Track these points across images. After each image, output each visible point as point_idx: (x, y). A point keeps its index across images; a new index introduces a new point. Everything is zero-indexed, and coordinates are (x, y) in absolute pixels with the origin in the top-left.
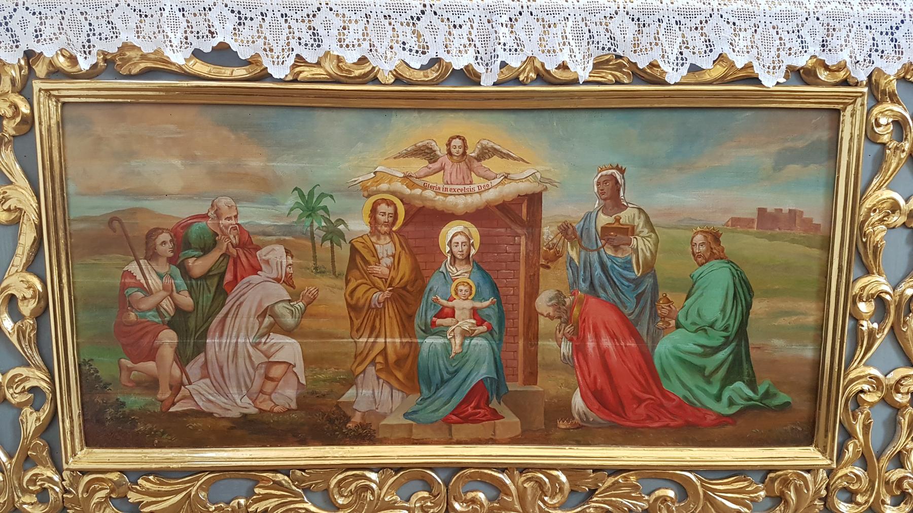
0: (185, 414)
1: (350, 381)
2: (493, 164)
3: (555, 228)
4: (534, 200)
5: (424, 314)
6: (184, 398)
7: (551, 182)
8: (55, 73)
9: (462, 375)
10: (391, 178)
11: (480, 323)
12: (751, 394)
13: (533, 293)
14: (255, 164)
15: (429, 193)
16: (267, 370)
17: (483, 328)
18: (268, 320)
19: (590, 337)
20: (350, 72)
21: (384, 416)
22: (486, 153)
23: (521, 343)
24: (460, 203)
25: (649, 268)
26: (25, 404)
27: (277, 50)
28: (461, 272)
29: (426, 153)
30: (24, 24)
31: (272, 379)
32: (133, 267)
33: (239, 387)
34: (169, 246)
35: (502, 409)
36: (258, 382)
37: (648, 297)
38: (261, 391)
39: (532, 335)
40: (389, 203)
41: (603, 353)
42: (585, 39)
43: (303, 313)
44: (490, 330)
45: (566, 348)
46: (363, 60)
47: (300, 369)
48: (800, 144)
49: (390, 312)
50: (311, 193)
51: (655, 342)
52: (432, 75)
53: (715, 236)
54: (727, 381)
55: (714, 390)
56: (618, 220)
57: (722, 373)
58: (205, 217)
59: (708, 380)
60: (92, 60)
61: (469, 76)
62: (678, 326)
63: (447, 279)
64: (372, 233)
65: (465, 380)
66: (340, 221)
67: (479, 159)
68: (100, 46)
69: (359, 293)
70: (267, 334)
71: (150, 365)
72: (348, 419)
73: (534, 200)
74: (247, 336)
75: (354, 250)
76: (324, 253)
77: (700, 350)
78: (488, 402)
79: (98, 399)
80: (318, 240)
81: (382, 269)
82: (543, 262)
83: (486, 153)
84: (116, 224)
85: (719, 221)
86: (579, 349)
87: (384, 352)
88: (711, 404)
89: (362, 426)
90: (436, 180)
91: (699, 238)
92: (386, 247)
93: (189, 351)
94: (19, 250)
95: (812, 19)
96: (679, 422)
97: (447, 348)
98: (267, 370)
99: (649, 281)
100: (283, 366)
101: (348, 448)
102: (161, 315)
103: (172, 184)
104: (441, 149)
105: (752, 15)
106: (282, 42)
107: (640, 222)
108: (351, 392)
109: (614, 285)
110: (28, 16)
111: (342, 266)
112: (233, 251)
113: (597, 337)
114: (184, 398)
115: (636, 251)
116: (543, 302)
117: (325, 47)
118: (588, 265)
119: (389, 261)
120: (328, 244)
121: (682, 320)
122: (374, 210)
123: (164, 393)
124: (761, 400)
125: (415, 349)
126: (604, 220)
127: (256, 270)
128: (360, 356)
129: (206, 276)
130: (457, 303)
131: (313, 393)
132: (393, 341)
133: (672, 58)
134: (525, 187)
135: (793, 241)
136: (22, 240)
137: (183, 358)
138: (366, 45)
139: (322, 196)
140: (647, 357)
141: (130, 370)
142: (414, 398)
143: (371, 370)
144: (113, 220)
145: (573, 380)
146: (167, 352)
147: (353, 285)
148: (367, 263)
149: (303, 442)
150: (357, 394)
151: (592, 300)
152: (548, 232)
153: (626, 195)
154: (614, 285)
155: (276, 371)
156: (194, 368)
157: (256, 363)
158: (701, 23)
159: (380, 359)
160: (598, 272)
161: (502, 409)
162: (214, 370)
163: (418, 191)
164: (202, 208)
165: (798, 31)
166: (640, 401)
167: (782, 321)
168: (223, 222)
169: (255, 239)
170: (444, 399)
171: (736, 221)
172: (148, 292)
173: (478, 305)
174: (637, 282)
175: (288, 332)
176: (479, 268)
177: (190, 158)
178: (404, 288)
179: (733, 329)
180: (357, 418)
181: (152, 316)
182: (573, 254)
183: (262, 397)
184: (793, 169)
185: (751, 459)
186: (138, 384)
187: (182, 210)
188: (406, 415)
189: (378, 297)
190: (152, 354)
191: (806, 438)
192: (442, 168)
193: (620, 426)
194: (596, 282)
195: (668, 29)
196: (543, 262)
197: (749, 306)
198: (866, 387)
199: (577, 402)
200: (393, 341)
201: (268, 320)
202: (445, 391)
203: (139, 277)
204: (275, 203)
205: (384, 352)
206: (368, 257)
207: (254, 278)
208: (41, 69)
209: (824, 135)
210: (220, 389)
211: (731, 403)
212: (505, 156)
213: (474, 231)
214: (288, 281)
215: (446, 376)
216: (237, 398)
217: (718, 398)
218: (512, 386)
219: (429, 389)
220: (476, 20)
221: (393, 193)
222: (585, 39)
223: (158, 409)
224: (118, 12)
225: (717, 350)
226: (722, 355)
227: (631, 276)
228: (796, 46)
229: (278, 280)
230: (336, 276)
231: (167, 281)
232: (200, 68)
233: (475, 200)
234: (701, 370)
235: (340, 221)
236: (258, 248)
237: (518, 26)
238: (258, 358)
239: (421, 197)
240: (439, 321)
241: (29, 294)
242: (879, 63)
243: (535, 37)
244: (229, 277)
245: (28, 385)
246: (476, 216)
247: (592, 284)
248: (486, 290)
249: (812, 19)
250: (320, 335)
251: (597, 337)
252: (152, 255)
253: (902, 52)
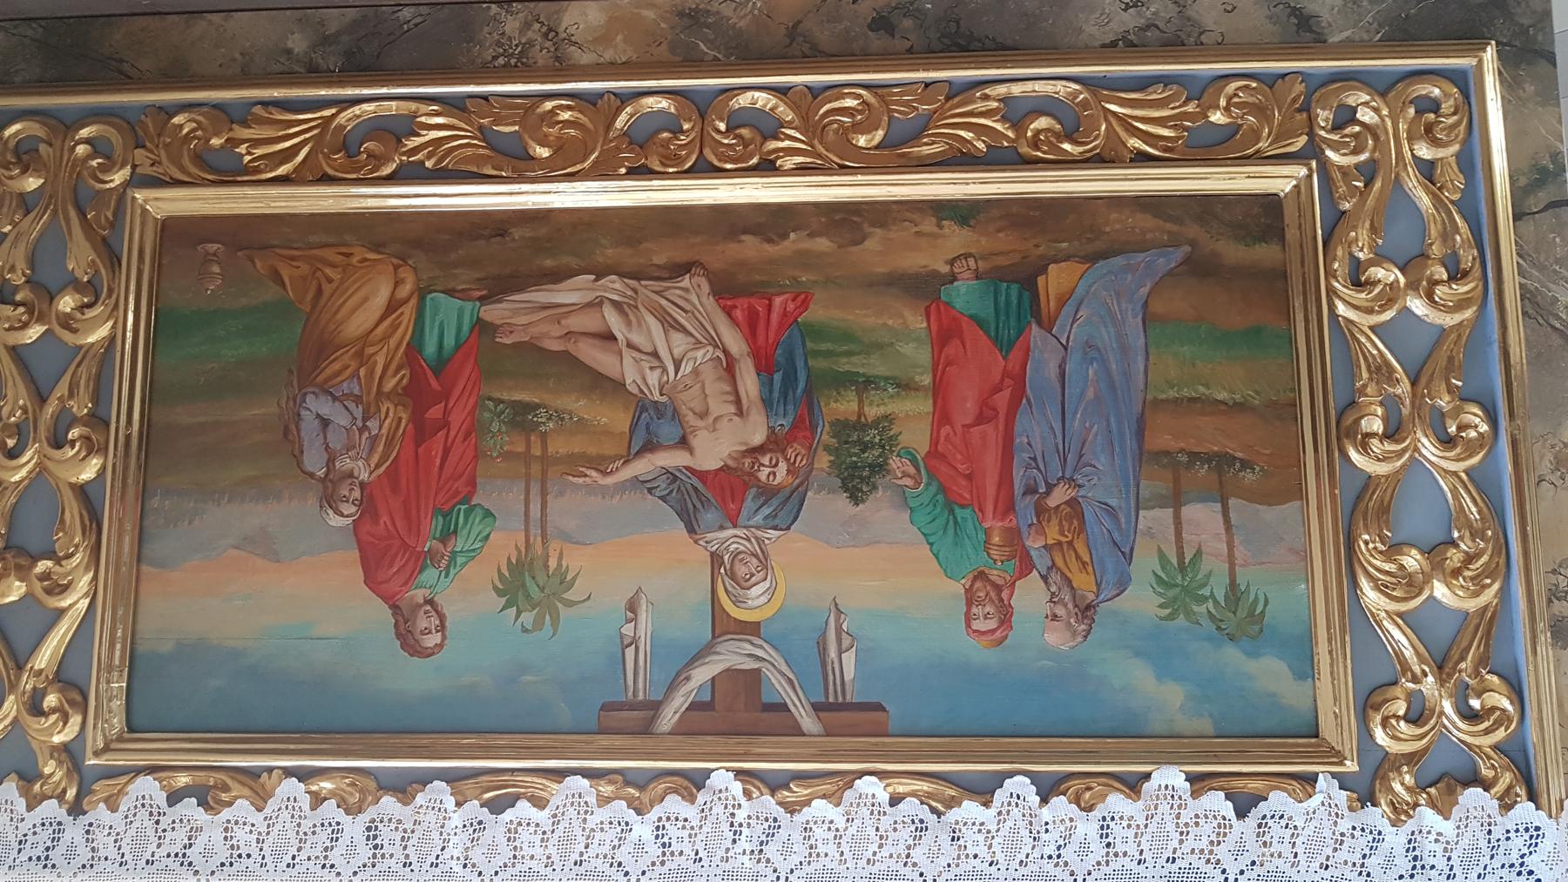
20: (353, 784)
42: (271, 840)
52: (799, 791)
158: (1107, 862)
165: (810, 854)
191: (175, 232)
220: (716, 860)
222: (271, 840)
224: (357, 863)
253: (927, 828)
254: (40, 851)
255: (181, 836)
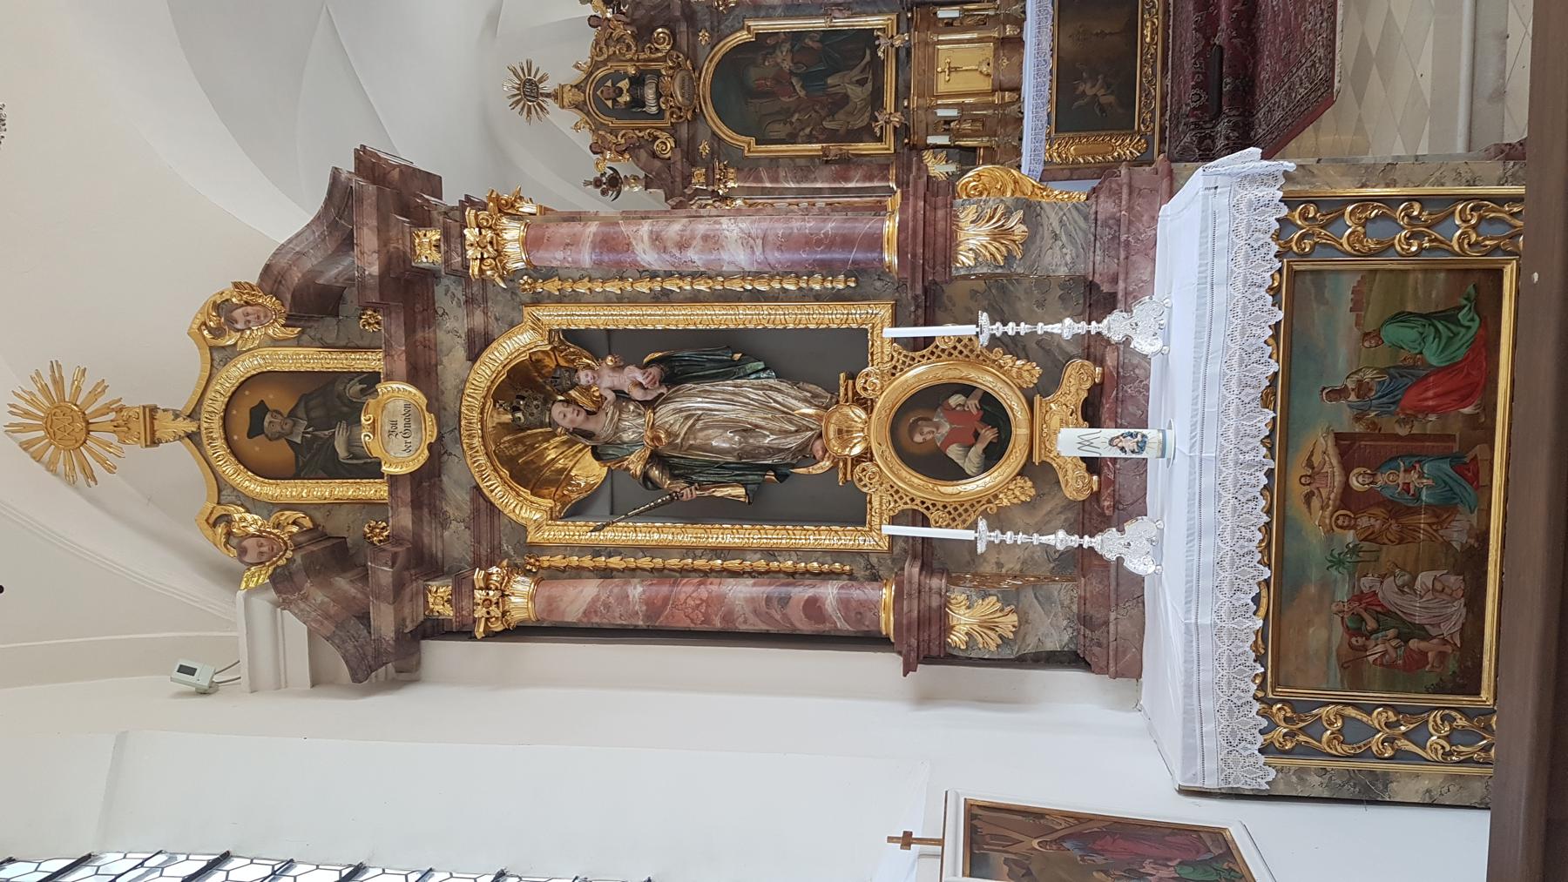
0: (1462, 638)
1: (1448, 544)
2: (1316, 460)
3: (1357, 425)
4: (1339, 437)
5: (1407, 500)
6: (1452, 638)
7: (1328, 428)
8: (1262, 687)
9: (1447, 479)
10: (1323, 517)
11: (1415, 468)
12: (1466, 309)
13: (1397, 437)
14: (1313, 590)
15: (1332, 496)
16: (1437, 591)
17: (1417, 466)
18: (1406, 589)
19: (1426, 403)
21: (1471, 525)
22: (1310, 464)
23: (1428, 444)
24: (1338, 479)
25: (1382, 371)
26: (1451, 726)
27: (1256, 573)
28: (1381, 479)
29: (1308, 497)
30: (1239, 698)
31: (1443, 589)
32: (1371, 659)
33: (1448, 607)
34: (1359, 639)
35: (1470, 455)
36: (1445, 597)
37: (1401, 371)
38: (1451, 595)
39: (1423, 437)
40: (1337, 519)
41: (1437, 396)
43: (1402, 570)
44: (1419, 462)
45: (1432, 418)
46: (1260, 530)
47: (1438, 574)
48: (1313, 291)
49: (1404, 520)
50: (1330, 561)
51: (1431, 366)
53: (1366, 335)
54: (1458, 323)
55: (1463, 331)
56: (1353, 390)
57: (1452, 327)
58: (1342, 618)
59: (1456, 335)
60: (1258, 665)
61: (1269, 474)
62: (1421, 353)
63: (1385, 486)
64: (1355, 529)
65: (1450, 477)
66: (1347, 546)
67: (1313, 468)
68: (1251, 662)
69: (1392, 539)
70: (1415, 591)
71: (1430, 654)
72: (1472, 546)
73: (1339, 437)
74: (1416, 601)
75: (1365, 540)
76: (1367, 557)
77: (1437, 340)
78: (1466, 464)
79: (1450, 686)
80: (1359, 559)
81: (1378, 524)
82: (1377, 432)
83: (1310, 464)
84: (1345, 665)
85: (1356, 333)
86: (1433, 410)
87: (1430, 525)
88: (1472, 332)
89: (1477, 540)
90: (1324, 492)
91: (1367, 344)
92: (1364, 522)
93: (1423, 633)
94: (1359, 717)
95: (1246, 294)
96: (1483, 350)
97: (1428, 487)
98: (1437, 591)
99: (1392, 371)
100: (1436, 582)
101: (1491, 547)
102: (1400, 646)
103: (1323, 634)
104: (1307, 489)
105: (1243, 327)
106: (1251, 570)
107: (1355, 377)
108: (1454, 544)
109: (1391, 392)
110: (1235, 695)
111: (1375, 546)
112: (1363, 605)
113: (1426, 399)
114: (1452, 638)
115: (1372, 379)
116: (1402, 431)
117: (1254, 549)
118: (1380, 406)
119: (1372, 520)
120: (1361, 554)
121: (1417, 351)
122: (1341, 527)
123: (1449, 649)
124: (1470, 302)
125: (1428, 506)
126: (1353, 397)
127: (1375, 594)
128: (1432, 538)
129: (1378, 621)
130: (1400, 481)
131: (814, 586)
132: (1423, 520)
133: (1265, 368)
134: (1331, 443)
135: (1371, 290)
136: (1354, 715)
137: (1427, 637)
138: (1253, 528)
139: (1331, 555)
140: (1439, 370)
141: (1433, 666)
142: (1460, 507)
143: (1441, 532)
144: (1343, 667)
145: (1453, 413)
146: (1423, 645)
147: (1386, 541)
148: (1373, 533)
149: (1486, 573)
150: (1197, 619)
151: (1402, 402)
152: (1359, 428)
153: (1338, 386)
154: (1391, 392)
155: (1439, 586)
156: (1433, 632)
157: (1432, 597)
159: (1434, 527)
160: (1384, 400)
161: (1470, 455)
162: (1435, 621)
163: (1331, 502)
164: (1338, 619)
166: (1469, 374)
167: (1420, 293)
168: (1346, 609)
169: (1356, 592)
170: (1462, 490)
171: (1357, 324)
172: (1385, 652)
173: (1402, 469)
174: (1392, 378)
175: (1415, 578)
176: (1380, 467)
177: (1309, 623)
178: (1390, 512)
179: (1424, 321)
180: (1472, 541)
181: (1401, 652)
182: (1373, 414)
183: (1454, 595)
184: (1327, 295)
185: (1510, 308)
186: (1442, 663)
187: (1339, 630)
188: (1472, 512)
189: (1394, 527)
190: (1424, 654)
191: (1498, 274)
192: (1318, 488)
193: (1485, 387)
194: (1392, 400)
195: (1249, 371)
196: (1377, 432)
197: (1411, 313)
198: (1466, 241)
199: (1467, 410)
200: (1423, 520)
201: (1406, 589)
202: (1457, 489)
203: (1377, 656)
204: (1335, 581)
205: (1430, 525)
206: (1370, 532)
207: (1380, 595)
208: (1260, 694)
209: (1308, 278)
210: (1448, 619)
211: (1472, 320)
212: (1312, 455)
213: (1356, 471)
214: (1383, 577)
215: (1447, 488)
216: (1454, 609)
217: (1469, 328)
218: (1456, 449)
219: (1454, 498)
221: (1332, 516)
223: (1458, 653)
225: (1437, 330)
226: (1440, 327)
227: (1388, 381)
228: (1261, 302)
229: (1382, 582)
230: (1380, 551)
231: (1379, 641)
232: (1262, 611)
233: (1337, 470)
234: (1450, 339)
235: (1347, 546)
236: (1362, 592)
237: (1245, 449)
238: (1430, 596)
239: (1334, 501)
240: (1412, 492)
241: (1385, 715)
242: (1272, 255)
243: (1250, 440)
244: (1379, 609)
245: (1439, 722)
246: (1347, 470)
247: (1393, 403)
248: (1393, 464)
249: (1246, 294)
250: (1417, 560)
251: (1426, 399)
252: (1365, 648)
254: (1259, 227)
255: (1243, 637)
